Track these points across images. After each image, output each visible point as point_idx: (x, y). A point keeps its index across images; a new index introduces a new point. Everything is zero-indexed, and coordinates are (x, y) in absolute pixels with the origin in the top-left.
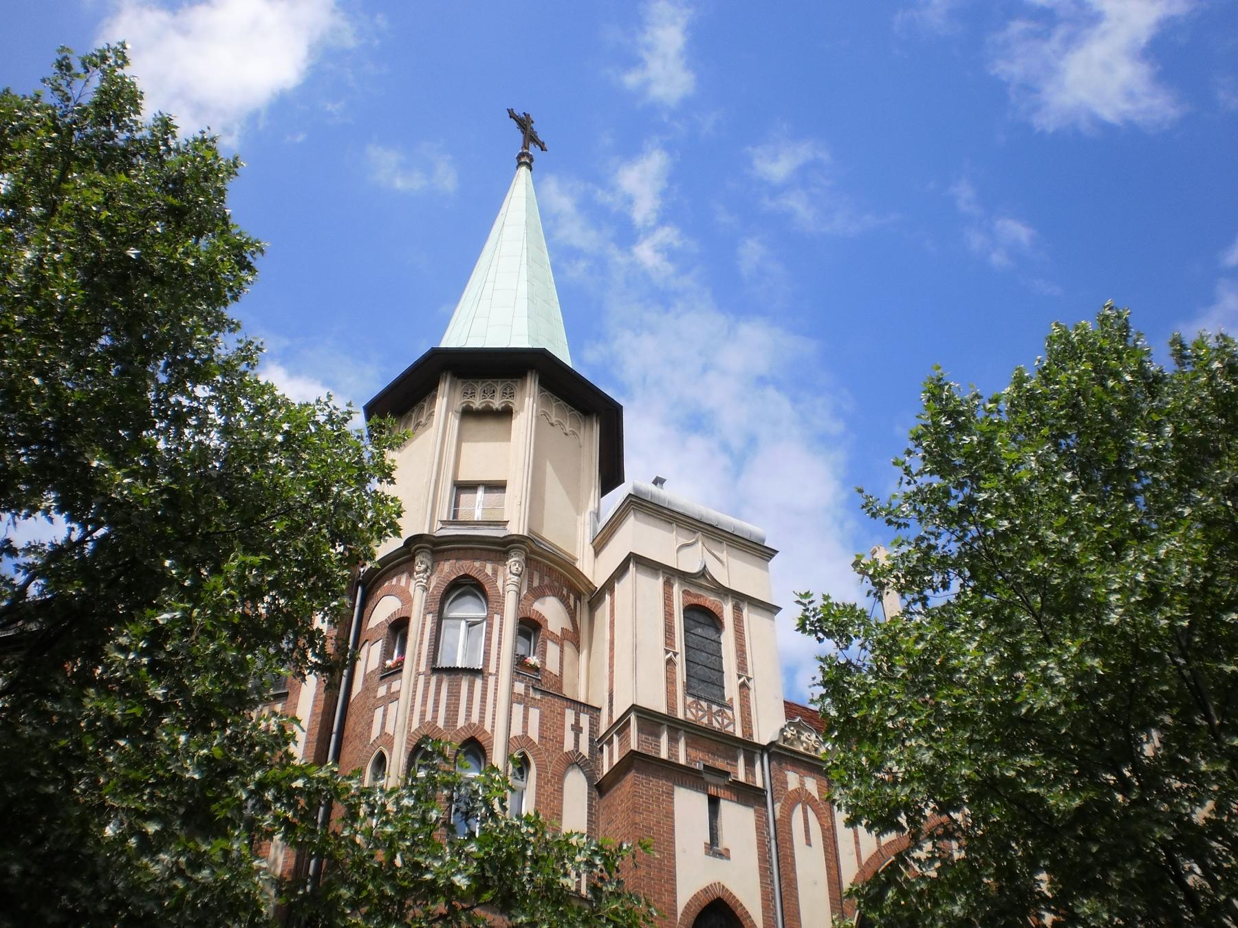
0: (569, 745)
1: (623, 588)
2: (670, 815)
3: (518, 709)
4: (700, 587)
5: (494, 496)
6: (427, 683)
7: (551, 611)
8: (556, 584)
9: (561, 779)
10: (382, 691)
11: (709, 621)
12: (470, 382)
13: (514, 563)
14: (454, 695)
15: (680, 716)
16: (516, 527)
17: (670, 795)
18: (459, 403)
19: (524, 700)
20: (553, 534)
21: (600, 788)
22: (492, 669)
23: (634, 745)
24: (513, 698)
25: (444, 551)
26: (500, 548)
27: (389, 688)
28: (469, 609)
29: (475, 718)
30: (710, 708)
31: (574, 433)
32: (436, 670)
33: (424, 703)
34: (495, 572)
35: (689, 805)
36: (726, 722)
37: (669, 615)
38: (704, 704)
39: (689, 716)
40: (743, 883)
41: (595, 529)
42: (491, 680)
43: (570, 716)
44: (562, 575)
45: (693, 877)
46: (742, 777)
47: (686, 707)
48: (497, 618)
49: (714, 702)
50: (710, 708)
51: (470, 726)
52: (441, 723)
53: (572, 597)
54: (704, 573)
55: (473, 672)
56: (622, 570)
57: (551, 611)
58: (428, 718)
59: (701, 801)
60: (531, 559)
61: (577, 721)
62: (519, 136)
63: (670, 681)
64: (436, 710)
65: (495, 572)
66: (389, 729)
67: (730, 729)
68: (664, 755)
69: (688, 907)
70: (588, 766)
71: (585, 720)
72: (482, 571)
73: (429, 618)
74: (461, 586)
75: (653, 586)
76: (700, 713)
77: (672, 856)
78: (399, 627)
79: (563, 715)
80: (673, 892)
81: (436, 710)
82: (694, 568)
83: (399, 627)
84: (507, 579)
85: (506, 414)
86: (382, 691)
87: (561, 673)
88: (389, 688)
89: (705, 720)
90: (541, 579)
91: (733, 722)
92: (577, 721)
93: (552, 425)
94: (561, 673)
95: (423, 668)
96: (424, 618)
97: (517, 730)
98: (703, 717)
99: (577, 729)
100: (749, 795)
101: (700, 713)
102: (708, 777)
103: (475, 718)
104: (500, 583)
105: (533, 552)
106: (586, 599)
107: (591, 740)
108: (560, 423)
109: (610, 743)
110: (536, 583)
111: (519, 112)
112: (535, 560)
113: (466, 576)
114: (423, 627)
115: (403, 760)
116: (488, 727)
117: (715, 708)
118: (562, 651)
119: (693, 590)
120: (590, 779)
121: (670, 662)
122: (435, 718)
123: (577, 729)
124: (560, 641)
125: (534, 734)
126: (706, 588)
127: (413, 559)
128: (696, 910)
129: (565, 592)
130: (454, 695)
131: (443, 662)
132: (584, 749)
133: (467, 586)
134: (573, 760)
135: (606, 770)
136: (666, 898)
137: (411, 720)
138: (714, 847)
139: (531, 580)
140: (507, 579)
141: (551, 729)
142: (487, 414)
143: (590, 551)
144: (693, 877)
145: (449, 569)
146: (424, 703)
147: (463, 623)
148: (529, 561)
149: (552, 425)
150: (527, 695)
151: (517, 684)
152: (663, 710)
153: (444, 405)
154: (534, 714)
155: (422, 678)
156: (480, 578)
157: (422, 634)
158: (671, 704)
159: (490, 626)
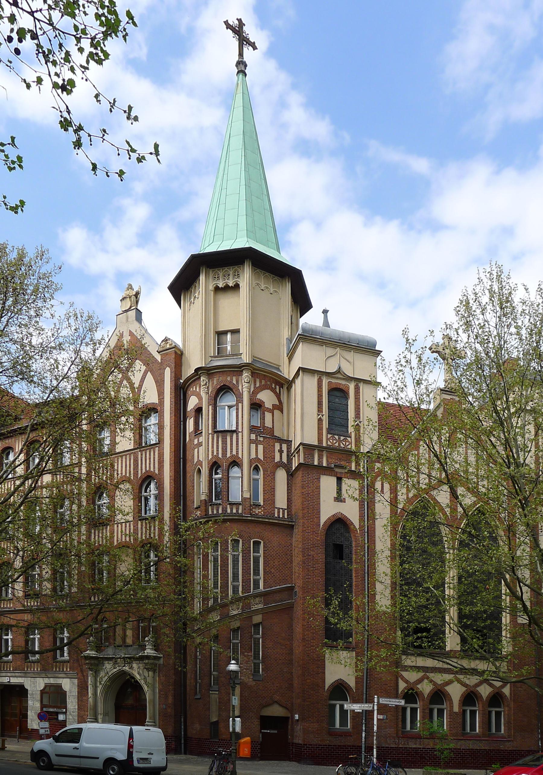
0: (277, 459)
1: (298, 381)
2: (318, 488)
3: (253, 446)
4: (337, 378)
5: (236, 335)
6: (213, 439)
7: (267, 397)
8: (268, 383)
9: (274, 474)
10: (196, 442)
11: (342, 394)
12: (216, 270)
13: (246, 375)
14: (224, 443)
15: (324, 444)
16: (246, 359)
17: (319, 479)
18: (211, 287)
19: (256, 442)
20: (267, 355)
21: (291, 475)
22: (240, 430)
23: (302, 461)
24: (251, 441)
25: (213, 373)
26: (238, 369)
27: (198, 440)
28: (229, 400)
29: (234, 453)
30: (339, 438)
31: (276, 292)
32: (215, 432)
33: (213, 447)
34: (237, 381)
35: (328, 484)
36: (347, 443)
37: (320, 396)
38: (337, 437)
39: (329, 443)
40: (351, 511)
41: (289, 347)
42: (240, 434)
43: (277, 446)
44: (271, 377)
45: (328, 509)
46: (353, 468)
47: (327, 439)
48: (240, 405)
49: (341, 436)
50: (339, 438)
51: (232, 456)
52: (220, 456)
53: (278, 387)
54: (339, 371)
55: (232, 432)
56: (297, 375)
57: (267, 397)
58: (215, 454)
59: (333, 480)
60: (255, 373)
61: (281, 448)
62: (235, 43)
63: (320, 429)
64: (218, 450)
65: (237, 381)
66: (201, 459)
67: (349, 447)
68: (316, 463)
69: (325, 522)
70: (287, 467)
71: (284, 447)
72: (231, 382)
73: (210, 407)
74: (224, 389)
75: (311, 382)
76: (335, 441)
77: (319, 504)
78: (199, 410)
79: (274, 446)
80: (319, 518)
81: (218, 450)
82: (332, 369)
83: (199, 410)
84: (245, 383)
85: (237, 287)
86: (196, 442)
87: (273, 426)
88: (198, 440)
89: (337, 444)
90: (260, 382)
91: (351, 443)
92: (281, 448)
93: (262, 290)
94: (273, 426)
95: (210, 432)
96: (208, 408)
97: (253, 456)
98: (336, 443)
99: (281, 451)
100: (355, 475)
101: (335, 441)
102: (337, 470)
103: (234, 453)
104: (240, 388)
105: (254, 369)
106: (285, 387)
107: (288, 455)
108: (267, 288)
109: (294, 456)
110: (258, 385)
111: (233, 22)
112: (256, 373)
113: (224, 385)
114: (208, 412)
115: (207, 472)
116: (240, 456)
117: (342, 438)
118: (273, 416)
119: (334, 381)
120: (287, 472)
121: (320, 420)
122: (218, 453)
123: (281, 451)
124: (272, 411)
125: (261, 456)
126: (341, 379)
127: (200, 378)
128: (329, 523)
129: (273, 386)
130: (224, 443)
131: (219, 428)
132: (285, 460)
133: (224, 389)
134: (280, 465)
135: (294, 468)
136: (315, 520)
137: (208, 455)
138: (339, 498)
139: (255, 384)
140: (245, 383)
141: (269, 453)
142: (227, 288)
143: (286, 359)
144: (328, 509)
145: (216, 382)
146: (213, 447)
147: (226, 407)
148: (253, 374)
149: (262, 290)
150: (257, 439)
151: (252, 435)
152: (316, 443)
153: (205, 283)
154: (261, 447)
155: (210, 435)
156: (231, 386)
157: (208, 415)
158: (320, 440)
159: (237, 409)
